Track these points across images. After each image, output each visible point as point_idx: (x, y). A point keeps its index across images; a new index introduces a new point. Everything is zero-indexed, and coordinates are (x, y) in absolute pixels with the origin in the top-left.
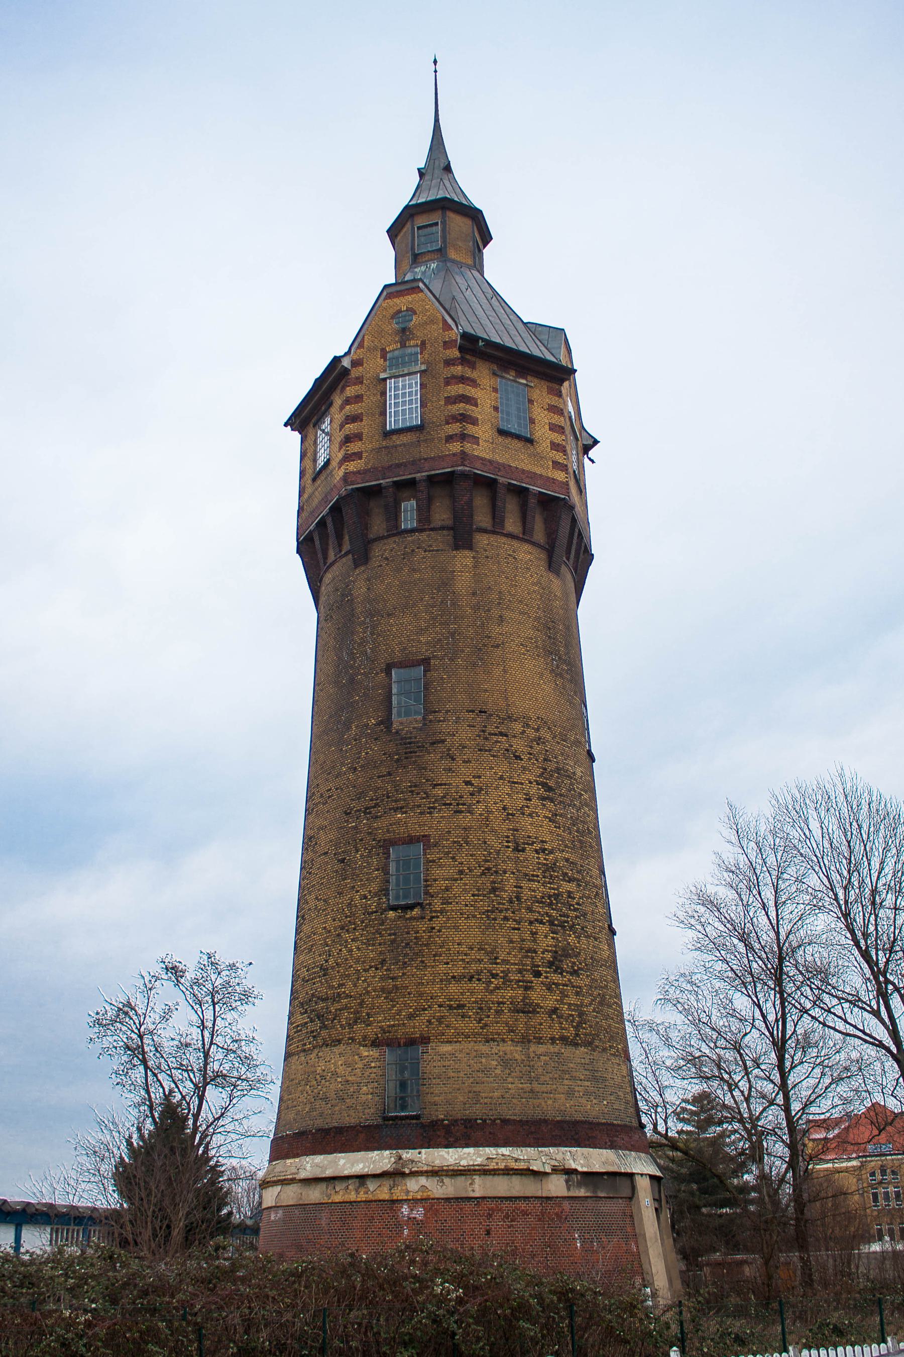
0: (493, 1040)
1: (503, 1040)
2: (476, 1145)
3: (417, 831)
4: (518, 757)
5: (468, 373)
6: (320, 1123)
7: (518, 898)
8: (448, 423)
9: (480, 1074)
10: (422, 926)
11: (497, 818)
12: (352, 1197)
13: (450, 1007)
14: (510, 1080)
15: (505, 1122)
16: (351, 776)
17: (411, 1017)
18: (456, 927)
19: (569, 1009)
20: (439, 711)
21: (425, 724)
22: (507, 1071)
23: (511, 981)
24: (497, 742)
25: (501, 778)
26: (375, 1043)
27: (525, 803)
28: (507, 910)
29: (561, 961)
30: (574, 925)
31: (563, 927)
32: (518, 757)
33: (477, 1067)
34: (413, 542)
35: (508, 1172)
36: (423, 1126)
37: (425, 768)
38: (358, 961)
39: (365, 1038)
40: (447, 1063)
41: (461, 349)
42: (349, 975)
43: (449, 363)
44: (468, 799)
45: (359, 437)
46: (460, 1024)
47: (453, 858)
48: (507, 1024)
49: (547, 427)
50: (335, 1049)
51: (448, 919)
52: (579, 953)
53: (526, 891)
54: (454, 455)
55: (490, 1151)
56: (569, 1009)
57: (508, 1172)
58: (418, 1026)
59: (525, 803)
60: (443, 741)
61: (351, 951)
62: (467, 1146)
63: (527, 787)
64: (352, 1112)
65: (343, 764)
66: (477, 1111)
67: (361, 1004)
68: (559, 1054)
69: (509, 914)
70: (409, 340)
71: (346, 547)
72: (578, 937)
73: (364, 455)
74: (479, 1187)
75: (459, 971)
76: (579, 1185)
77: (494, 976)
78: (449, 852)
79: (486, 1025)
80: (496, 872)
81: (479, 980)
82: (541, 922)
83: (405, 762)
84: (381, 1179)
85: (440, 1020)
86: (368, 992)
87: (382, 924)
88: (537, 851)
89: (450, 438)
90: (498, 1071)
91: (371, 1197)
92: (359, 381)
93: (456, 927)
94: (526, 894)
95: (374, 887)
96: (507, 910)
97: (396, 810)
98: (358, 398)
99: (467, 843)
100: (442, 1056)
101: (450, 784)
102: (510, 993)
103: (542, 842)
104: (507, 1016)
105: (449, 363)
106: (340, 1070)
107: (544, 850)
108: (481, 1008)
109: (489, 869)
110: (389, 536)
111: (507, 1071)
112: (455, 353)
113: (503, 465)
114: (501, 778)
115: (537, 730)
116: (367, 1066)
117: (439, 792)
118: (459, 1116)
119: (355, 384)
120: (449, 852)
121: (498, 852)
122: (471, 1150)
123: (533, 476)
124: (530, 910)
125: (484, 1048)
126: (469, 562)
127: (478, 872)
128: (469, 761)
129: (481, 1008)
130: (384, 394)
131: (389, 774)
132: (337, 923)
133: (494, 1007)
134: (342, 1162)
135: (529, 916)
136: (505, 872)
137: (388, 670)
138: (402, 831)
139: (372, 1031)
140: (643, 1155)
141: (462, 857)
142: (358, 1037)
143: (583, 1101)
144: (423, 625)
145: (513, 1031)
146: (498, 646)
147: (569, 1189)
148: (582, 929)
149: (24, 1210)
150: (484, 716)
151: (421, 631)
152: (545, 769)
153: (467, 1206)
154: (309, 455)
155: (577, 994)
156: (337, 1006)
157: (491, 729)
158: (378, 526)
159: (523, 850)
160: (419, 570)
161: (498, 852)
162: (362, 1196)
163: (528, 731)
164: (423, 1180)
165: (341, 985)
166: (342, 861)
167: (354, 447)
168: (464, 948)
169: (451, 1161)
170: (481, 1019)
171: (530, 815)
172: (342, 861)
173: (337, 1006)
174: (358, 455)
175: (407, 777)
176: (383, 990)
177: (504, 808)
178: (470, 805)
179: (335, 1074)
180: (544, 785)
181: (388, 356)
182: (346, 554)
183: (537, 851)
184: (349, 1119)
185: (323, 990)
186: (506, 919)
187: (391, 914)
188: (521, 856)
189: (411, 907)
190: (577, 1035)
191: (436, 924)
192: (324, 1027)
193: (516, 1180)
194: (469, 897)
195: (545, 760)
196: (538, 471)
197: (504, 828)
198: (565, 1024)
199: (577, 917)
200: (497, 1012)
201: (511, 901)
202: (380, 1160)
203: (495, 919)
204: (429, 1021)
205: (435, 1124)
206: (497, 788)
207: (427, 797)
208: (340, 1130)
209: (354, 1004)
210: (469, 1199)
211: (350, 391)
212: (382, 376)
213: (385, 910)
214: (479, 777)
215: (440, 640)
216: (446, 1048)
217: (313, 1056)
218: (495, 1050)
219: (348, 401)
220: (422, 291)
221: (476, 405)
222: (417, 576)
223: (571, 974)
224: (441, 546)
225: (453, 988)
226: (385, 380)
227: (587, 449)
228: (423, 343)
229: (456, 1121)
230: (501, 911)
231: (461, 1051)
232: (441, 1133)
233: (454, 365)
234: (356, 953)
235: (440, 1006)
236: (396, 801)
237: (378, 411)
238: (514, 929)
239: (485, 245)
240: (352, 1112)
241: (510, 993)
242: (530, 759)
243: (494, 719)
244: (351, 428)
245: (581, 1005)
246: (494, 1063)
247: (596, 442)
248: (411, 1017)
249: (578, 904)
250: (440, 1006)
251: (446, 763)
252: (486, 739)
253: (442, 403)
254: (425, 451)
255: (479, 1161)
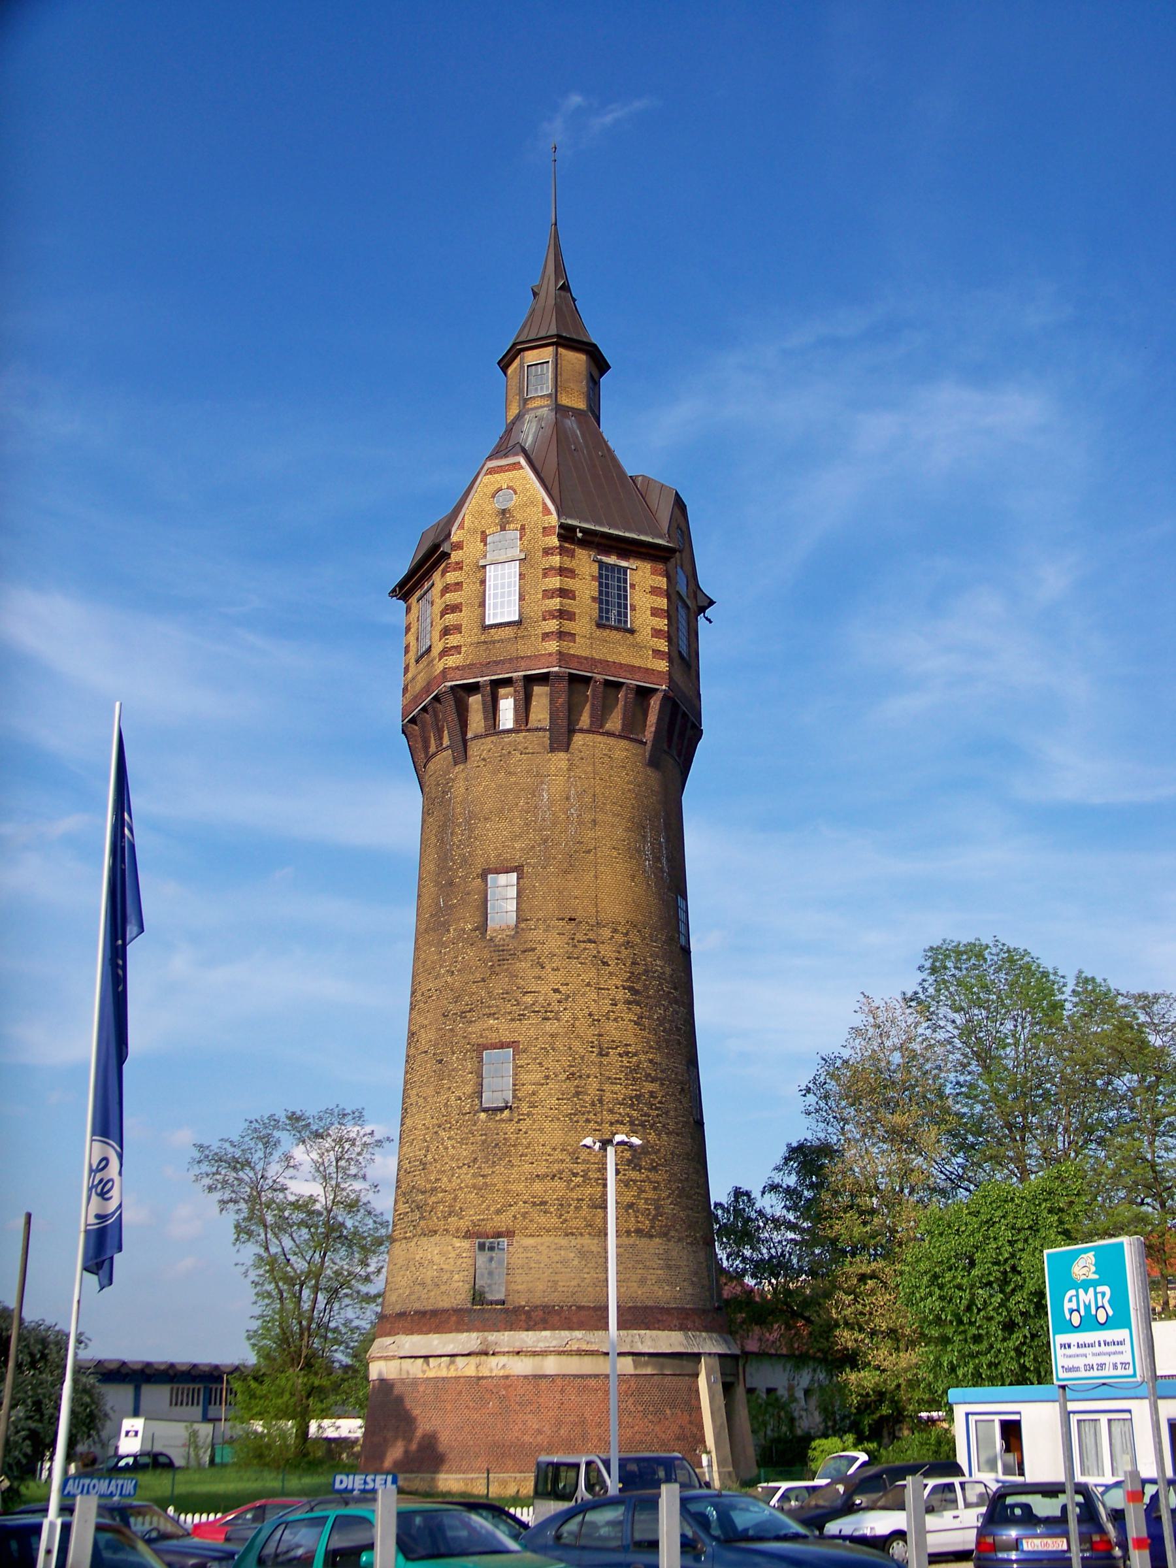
0: (572, 1234)
1: (581, 1234)
2: (553, 1328)
3: (507, 1038)
4: (605, 964)
5: (568, 563)
6: (417, 1306)
7: (601, 1101)
8: (544, 620)
9: (559, 1265)
10: (511, 1128)
11: (582, 1026)
12: (444, 1373)
13: (534, 1204)
14: (586, 1270)
15: (580, 1308)
16: (449, 979)
17: (498, 1212)
18: (541, 1130)
19: (646, 1203)
20: (531, 920)
21: (517, 932)
22: (584, 1262)
23: (590, 1179)
24: (585, 949)
25: (588, 985)
26: (468, 1235)
27: (610, 1008)
28: (589, 1112)
29: (639, 1159)
30: (655, 1123)
31: (644, 1126)
32: (605, 964)
33: (556, 1258)
34: (510, 743)
35: (580, 1353)
36: (507, 1311)
37: (517, 976)
38: (452, 1159)
39: (458, 1230)
40: (529, 1255)
41: (560, 536)
42: (444, 1171)
43: (547, 552)
44: (555, 1006)
45: (458, 629)
46: (542, 1220)
47: (540, 1064)
48: (585, 1219)
49: (649, 612)
50: (432, 1239)
51: (534, 1121)
52: (659, 1150)
53: (608, 1094)
54: (550, 654)
55: (566, 1334)
56: (646, 1203)
57: (580, 1353)
58: (502, 1222)
59: (610, 1008)
60: (533, 950)
61: (446, 1148)
62: (545, 1329)
63: (613, 991)
64: (445, 1297)
65: (441, 966)
66: (554, 1298)
67: (455, 1199)
68: (633, 1246)
69: (591, 1116)
70: (508, 523)
71: (446, 742)
72: (659, 1135)
73: (463, 649)
74: (551, 1366)
75: (542, 1171)
76: (646, 1364)
77: (575, 1175)
78: (535, 1059)
79: (566, 1220)
80: (580, 1077)
81: (561, 1178)
82: (622, 1123)
83: (497, 969)
84: (469, 1358)
85: (524, 1215)
86: (461, 1188)
87: (475, 1125)
88: (620, 1055)
89: (546, 636)
90: (575, 1263)
91: (459, 1374)
92: (459, 566)
93: (541, 1130)
94: (608, 1096)
95: (468, 1089)
96: (589, 1112)
97: (489, 1015)
98: (458, 586)
99: (553, 1049)
100: (526, 1249)
101: (538, 992)
102: (589, 1191)
103: (626, 1045)
104: (585, 1210)
105: (547, 552)
106: (436, 1259)
107: (627, 1053)
108: (562, 1205)
109: (573, 1074)
110: (487, 735)
111: (584, 1262)
112: (554, 541)
113: (601, 661)
114: (588, 985)
115: (627, 934)
116: (459, 1256)
117: (529, 999)
118: (538, 1303)
119: (455, 570)
120: (535, 1059)
121: (582, 1058)
122: (547, 1333)
123: (632, 669)
124: (611, 1111)
125: (563, 1241)
126: (564, 765)
127: (563, 1076)
128: (558, 969)
129: (562, 1205)
130: (483, 582)
131: (483, 980)
132: (435, 1121)
133: (574, 1203)
134: (436, 1342)
135: (610, 1117)
136: (588, 1076)
137: (484, 876)
138: (493, 1037)
139: (464, 1224)
140: (714, 1335)
141: (549, 1063)
142: (452, 1229)
143: (656, 1288)
144: (517, 830)
145: (590, 1226)
146: (589, 852)
147: (636, 1368)
148: (664, 1126)
149: (142, 1371)
150: (573, 924)
151: (516, 837)
152: (632, 973)
153: (543, 1384)
154: (412, 630)
155: (655, 1189)
156: (434, 1199)
157: (579, 937)
158: (476, 721)
159: (607, 1054)
160: (515, 774)
161: (582, 1058)
162: (452, 1373)
163: (616, 936)
164: (503, 1360)
165: (437, 1180)
166: (440, 1061)
167: (453, 640)
168: (548, 1149)
169: (530, 1343)
170: (561, 1215)
171: (615, 1020)
172: (440, 1061)
173: (434, 1199)
174: (457, 649)
175: (499, 985)
176: (474, 1186)
177: (590, 1015)
178: (558, 1012)
179: (431, 1262)
180: (630, 989)
181: (489, 539)
182: (445, 749)
183: (620, 1055)
184: (445, 1303)
185: (421, 1183)
186: (588, 1121)
187: (483, 1115)
188: (605, 1060)
189: (501, 1110)
190: (652, 1227)
191: (523, 1126)
192: (422, 1218)
193: (587, 1359)
194: (554, 1101)
195: (633, 963)
196: (637, 662)
197: (591, 1033)
198: (641, 1218)
199: (658, 1116)
200: (576, 1208)
201: (593, 1104)
202: (469, 1340)
203: (577, 1122)
204: (514, 1216)
205: (518, 1310)
206: (584, 995)
207: (518, 1004)
208: (435, 1313)
209: (449, 1197)
210: (546, 1376)
211: (451, 577)
212: (482, 563)
213: (477, 1112)
214: (567, 984)
215: (533, 847)
216: (530, 1241)
217: (413, 1244)
218: (573, 1243)
219: (446, 589)
220: (522, 468)
221: (574, 598)
222: (513, 779)
223: (650, 1170)
224: (537, 749)
225: (538, 1186)
226: (484, 567)
227: (702, 610)
228: (523, 528)
229: (537, 1307)
230: (583, 1114)
231: (542, 1244)
232: (523, 1317)
233: (552, 554)
234: (451, 1151)
235: (525, 1202)
236: (489, 1007)
237: (477, 602)
238: (595, 1130)
239: (602, 374)
240: (445, 1297)
241: (589, 1191)
242: (617, 964)
243: (584, 926)
244: (451, 619)
245: (659, 1199)
246: (572, 1255)
247: (712, 603)
248: (498, 1212)
249: (660, 1102)
250: (525, 1202)
251: (537, 971)
252: (575, 946)
253: (540, 596)
254: (523, 649)
255: (554, 1343)
